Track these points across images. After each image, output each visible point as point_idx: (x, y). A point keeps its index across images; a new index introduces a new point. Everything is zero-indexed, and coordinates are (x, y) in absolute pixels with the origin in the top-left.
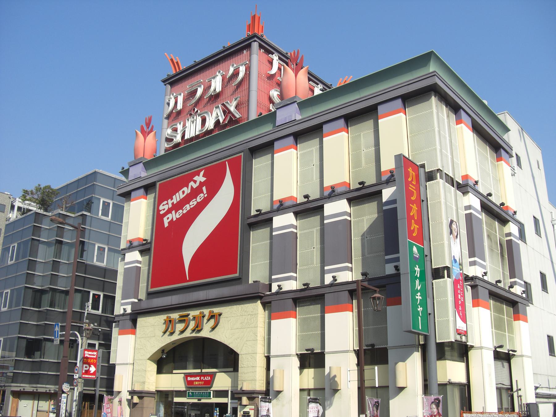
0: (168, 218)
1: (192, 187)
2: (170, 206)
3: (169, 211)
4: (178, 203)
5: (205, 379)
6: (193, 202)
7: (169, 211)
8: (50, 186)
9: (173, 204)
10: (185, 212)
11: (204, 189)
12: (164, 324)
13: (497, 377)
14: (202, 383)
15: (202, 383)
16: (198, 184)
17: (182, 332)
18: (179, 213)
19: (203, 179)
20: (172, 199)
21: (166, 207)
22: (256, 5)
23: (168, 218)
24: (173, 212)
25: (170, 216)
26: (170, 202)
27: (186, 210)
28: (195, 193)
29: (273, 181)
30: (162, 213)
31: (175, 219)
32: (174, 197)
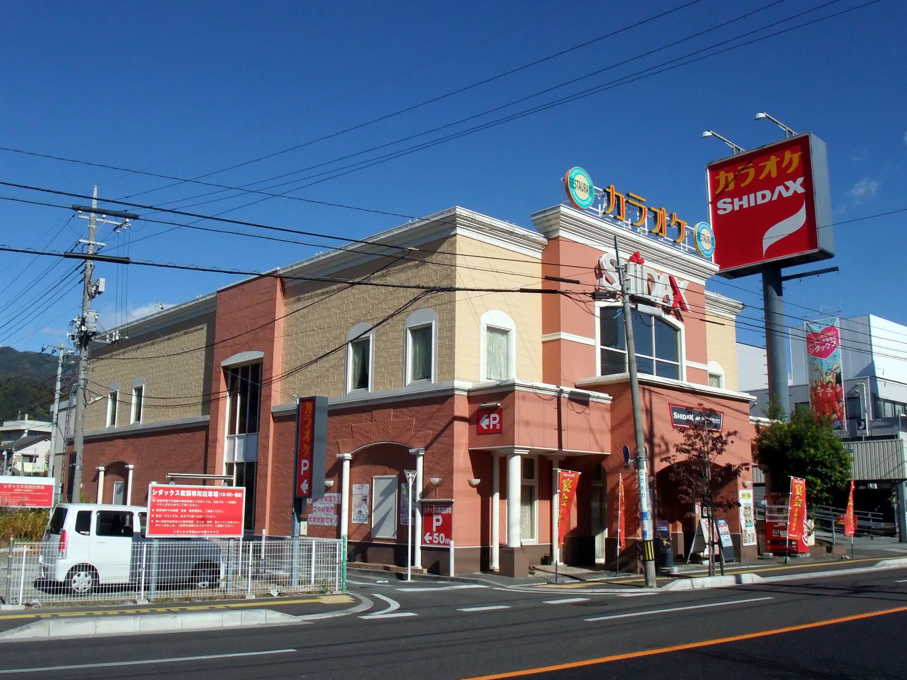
1: (780, 193)
16: (790, 193)
20: (741, 199)
32: (745, 198)
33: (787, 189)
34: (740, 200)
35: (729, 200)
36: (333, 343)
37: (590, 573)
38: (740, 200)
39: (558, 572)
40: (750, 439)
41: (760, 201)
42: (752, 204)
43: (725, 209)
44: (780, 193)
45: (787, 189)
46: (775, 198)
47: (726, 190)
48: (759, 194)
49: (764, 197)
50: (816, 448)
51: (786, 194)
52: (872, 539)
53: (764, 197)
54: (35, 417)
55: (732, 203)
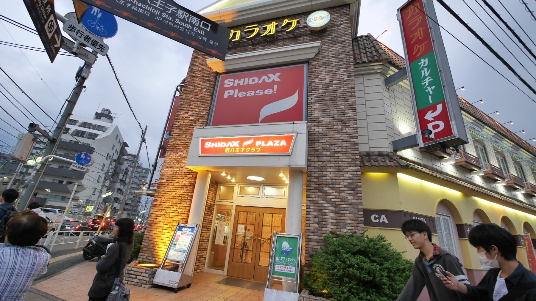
0: (229, 93)
1: (264, 80)
2: (236, 84)
3: (233, 88)
4: (244, 85)
5: (369, 297)
6: (259, 94)
7: (233, 88)
8: (478, 252)
9: (239, 84)
10: (248, 95)
11: (275, 87)
12: (72, 114)
13: (310, 142)
14: (294, 260)
15: (294, 260)
16: (270, 80)
17: (418, 33)
18: (242, 93)
19: (277, 80)
20: (239, 80)
21: (231, 84)
22: (200, 158)
23: (229, 93)
24: (237, 91)
25: (232, 92)
26: (237, 82)
27: (250, 94)
28: (265, 86)
29: (479, 36)
30: (225, 86)
31: (236, 96)
32: (242, 80)
33: (269, 78)
34: (239, 84)
35: (232, 80)
36: (354, 282)
37: (444, 72)
38: (239, 84)
39: (235, 250)
40: (86, 199)
41: (251, 82)
42: (246, 83)
43: (228, 85)
44: (264, 80)
45: (269, 78)
46: (261, 82)
47: (233, 40)
48: (251, 79)
49: (254, 80)
50: (377, 268)
51: (267, 80)
52: (85, 87)
53: (254, 80)
54: (33, 246)
55: (234, 82)
